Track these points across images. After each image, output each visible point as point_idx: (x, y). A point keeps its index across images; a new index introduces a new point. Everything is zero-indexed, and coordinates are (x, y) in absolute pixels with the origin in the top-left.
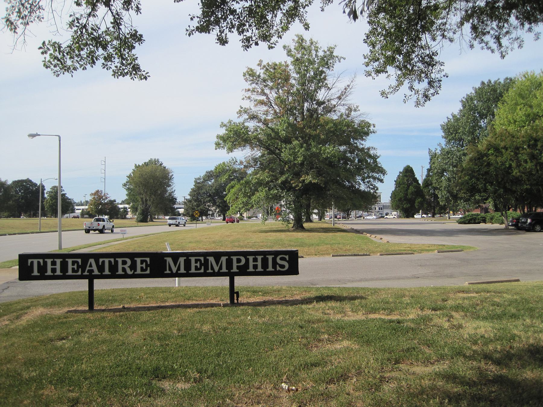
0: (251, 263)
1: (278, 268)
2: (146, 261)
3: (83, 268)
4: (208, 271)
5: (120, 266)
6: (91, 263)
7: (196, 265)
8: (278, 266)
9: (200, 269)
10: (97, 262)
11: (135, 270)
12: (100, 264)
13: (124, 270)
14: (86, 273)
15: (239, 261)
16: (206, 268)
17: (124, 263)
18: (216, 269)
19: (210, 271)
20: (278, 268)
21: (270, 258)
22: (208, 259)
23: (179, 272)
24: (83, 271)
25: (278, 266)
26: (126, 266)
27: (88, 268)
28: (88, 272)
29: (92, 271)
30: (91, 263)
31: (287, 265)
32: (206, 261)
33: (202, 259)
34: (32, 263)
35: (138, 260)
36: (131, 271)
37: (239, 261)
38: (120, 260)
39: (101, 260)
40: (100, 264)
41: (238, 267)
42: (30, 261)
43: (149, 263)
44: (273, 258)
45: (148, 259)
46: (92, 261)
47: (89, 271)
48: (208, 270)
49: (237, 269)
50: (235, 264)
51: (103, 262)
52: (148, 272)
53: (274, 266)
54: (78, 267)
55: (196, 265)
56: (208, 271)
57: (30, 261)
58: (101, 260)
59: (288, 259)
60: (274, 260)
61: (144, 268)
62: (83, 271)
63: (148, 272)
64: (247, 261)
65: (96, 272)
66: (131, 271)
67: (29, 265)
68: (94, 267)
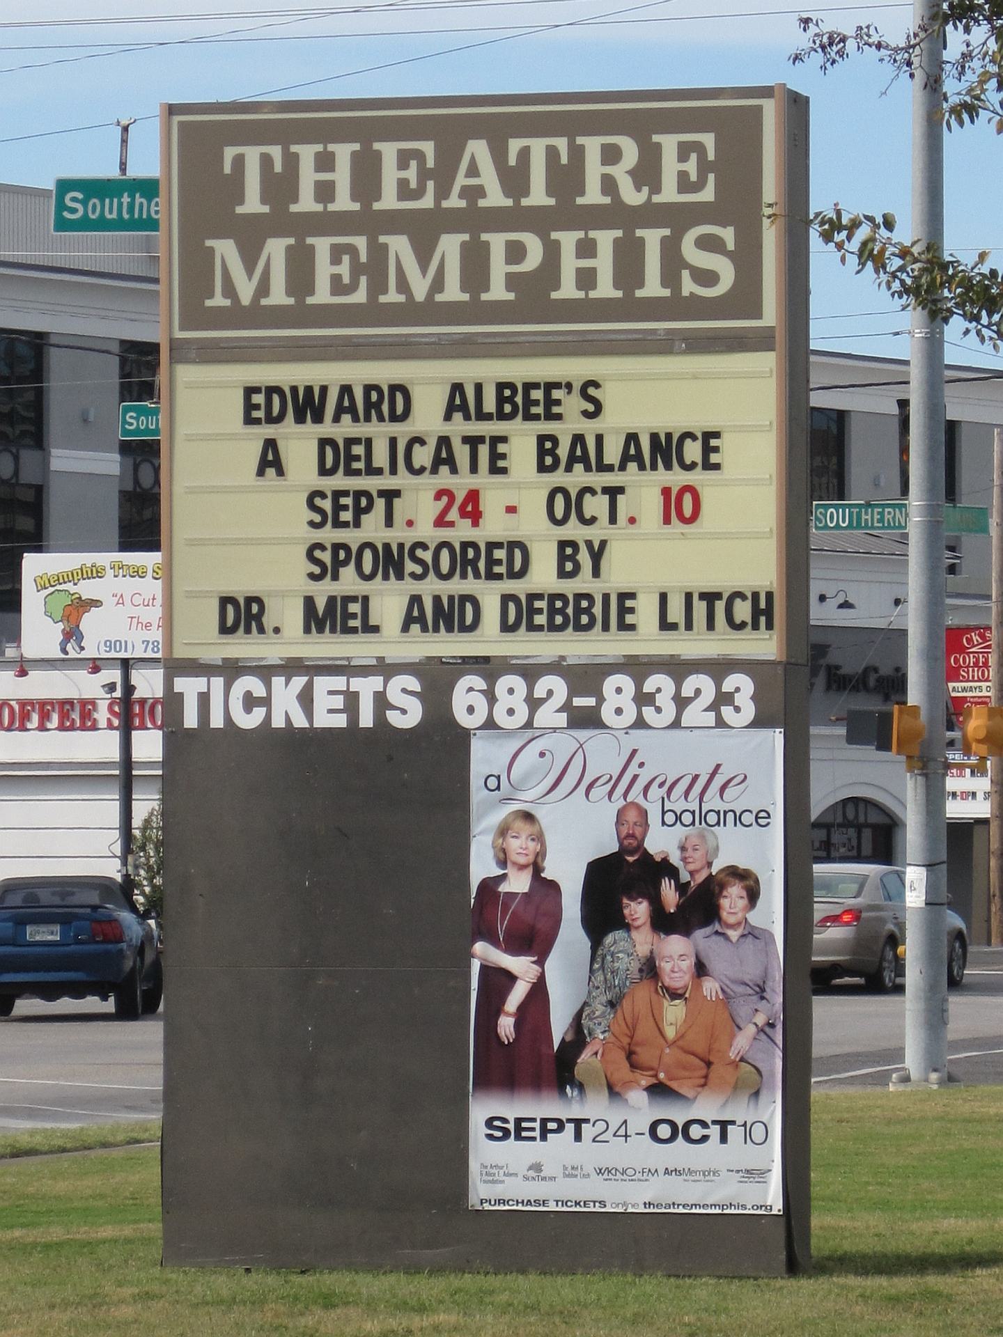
0: (570, 264)
1: (689, 286)
2: (699, 148)
3: (443, 175)
4: (383, 299)
5: (594, 170)
6: (473, 158)
7: (336, 270)
8: (686, 274)
9: (352, 288)
10: (499, 154)
11: (656, 188)
12: (512, 161)
13: (609, 185)
14: (454, 201)
15: (516, 252)
16: (377, 286)
17: (611, 155)
18: (420, 288)
19: (392, 296)
20: (689, 286)
21: (653, 238)
22: (385, 247)
23: (264, 302)
24: (443, 193)
25: (686, 274)
26: (620, 173)
27: (461, 180)
28: (461, 196)
29: (480, 192)
30: (473, 158)
31: (726, 270)
32: (379, 253)
33: (361, 242)
34: (239, 161)
35: (669, 143)
36: (639, 190)
37: (516, 252)
38: (592, 146)
39: (515, 145)
40: (512, 161)
41: (512, 281)
42: (230, 153)
43: (711, 156)
44: (664, 240)
45: (708, 140)
46: (478, 149)
47: (466, 192)
48: (385, 291)
49: (509, 288)
50: (499, 268)
51: (525, 154)
52: (707, 194)
53: (670, 276)
54: (424, 174)
55: (336, 270)
56: (383, 299)
57: (230, 153)
58: (515, 145)
59: (731, 246)
60: (671, 251)
61: (693, 177)
62: (443, 193)
63: (707, 194)
64: (552, 252)
65: (495, 197)
66: (639, 190)
67: (227, 169)
68: (489, 178)
